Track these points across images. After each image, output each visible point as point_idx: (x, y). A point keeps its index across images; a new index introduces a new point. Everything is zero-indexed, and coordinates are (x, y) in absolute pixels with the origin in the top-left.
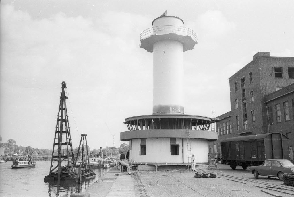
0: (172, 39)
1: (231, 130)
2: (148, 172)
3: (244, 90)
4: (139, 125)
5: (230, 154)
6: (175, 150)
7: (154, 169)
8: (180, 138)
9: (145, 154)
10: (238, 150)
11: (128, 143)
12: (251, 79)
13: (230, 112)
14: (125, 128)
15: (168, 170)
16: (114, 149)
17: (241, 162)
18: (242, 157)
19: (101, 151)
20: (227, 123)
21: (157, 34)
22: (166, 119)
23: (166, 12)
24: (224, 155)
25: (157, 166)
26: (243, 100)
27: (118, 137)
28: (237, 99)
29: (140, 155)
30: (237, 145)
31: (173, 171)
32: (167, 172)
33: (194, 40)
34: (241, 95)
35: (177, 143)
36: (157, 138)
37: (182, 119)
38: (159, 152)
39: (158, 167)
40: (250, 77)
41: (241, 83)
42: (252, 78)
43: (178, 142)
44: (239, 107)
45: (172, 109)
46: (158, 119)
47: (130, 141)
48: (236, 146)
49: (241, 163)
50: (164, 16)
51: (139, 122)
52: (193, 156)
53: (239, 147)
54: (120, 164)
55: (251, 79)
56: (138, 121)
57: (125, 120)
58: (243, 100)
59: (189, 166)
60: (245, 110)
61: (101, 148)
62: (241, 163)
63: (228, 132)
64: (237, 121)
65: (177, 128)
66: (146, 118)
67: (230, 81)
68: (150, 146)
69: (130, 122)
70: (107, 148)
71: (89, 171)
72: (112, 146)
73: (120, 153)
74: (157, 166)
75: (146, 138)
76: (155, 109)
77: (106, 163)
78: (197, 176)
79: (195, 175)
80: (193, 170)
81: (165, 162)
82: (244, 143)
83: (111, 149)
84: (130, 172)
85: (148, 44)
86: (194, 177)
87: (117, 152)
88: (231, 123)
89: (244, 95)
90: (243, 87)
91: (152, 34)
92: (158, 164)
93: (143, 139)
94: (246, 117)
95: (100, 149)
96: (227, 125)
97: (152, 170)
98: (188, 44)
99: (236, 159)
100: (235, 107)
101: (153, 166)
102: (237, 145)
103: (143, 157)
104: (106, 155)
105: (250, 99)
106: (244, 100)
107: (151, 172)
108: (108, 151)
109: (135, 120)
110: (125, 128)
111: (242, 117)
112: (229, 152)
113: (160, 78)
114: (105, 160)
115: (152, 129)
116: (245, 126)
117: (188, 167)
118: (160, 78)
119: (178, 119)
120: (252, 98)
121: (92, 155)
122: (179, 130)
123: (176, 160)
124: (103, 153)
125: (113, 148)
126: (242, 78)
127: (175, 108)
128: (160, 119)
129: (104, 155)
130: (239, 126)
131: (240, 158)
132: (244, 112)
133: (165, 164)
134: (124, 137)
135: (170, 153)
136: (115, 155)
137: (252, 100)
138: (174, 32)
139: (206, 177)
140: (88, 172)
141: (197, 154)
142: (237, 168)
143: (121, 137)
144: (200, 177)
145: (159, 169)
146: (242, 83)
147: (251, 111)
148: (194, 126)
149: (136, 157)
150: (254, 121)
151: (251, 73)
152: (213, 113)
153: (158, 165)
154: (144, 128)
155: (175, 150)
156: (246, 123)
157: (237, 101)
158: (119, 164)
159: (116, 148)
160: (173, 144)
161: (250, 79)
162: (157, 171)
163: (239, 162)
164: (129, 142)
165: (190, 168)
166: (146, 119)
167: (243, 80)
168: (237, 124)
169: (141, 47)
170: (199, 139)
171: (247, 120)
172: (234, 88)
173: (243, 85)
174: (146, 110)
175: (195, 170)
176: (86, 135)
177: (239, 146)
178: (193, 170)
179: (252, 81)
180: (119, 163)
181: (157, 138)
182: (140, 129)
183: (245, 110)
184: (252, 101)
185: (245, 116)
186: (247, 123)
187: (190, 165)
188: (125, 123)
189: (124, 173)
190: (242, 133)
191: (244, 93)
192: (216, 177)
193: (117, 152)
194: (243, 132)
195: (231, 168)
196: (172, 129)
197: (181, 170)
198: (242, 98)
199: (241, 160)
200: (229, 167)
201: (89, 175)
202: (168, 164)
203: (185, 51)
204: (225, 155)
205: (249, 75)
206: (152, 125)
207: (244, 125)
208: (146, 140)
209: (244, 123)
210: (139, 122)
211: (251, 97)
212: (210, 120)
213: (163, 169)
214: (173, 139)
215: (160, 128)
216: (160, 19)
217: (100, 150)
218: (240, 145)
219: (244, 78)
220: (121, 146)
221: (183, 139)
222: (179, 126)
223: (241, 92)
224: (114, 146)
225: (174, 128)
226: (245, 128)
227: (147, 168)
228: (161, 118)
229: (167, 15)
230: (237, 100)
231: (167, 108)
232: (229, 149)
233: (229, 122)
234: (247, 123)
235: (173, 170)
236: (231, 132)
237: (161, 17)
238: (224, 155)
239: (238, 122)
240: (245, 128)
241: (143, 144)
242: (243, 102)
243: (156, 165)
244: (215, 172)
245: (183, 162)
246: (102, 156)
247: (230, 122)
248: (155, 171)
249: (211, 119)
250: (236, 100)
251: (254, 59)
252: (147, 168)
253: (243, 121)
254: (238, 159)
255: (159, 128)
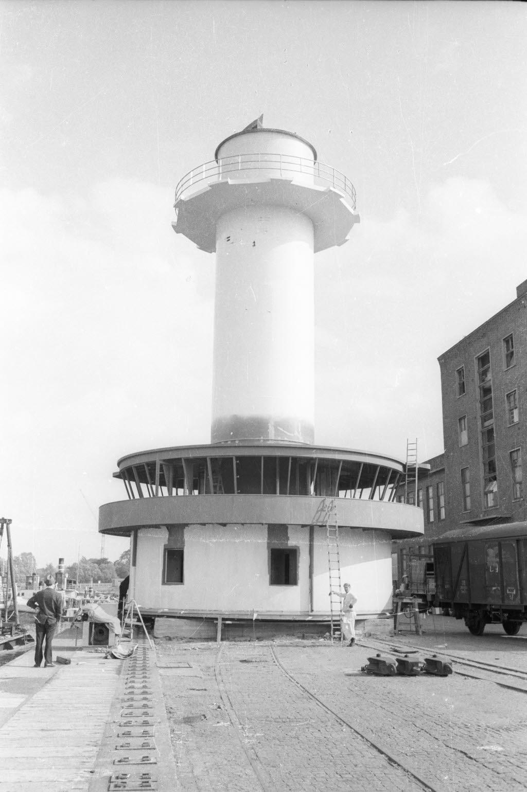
0: (276, 200)
1: (443, 511)
2: (193, 645)
3: (486, 391)
4: (162, 483)
5: (464, 582)
6: (283, 568)
7: (211, 634)
8: (303, 526)
9: (181, 580)
10: (494, 568)
11: (123, 544)
12: (510, 355)
13: (442, 456)
14: (118, 491)
15: (259, 634)
16: (103, 565)
17: (505, 611)
18: (512, 592)
19: (63, 570)
20: (431, 490)
21: (230, 182)
22: (256, 459)
23: (261, 118)
24: (443, 586)
25: (220, 622)
26: (484, 419)
27: (93, 522)
28: (464, 417)
29: (164, 583)
30: (492, 552)
31: (277, 641)
32: (256, 643)
33: (352, 210)
34: (478, 405)
35: (292, 543)
36: (224, 525)
37: (310, 461)
38: (227, 572)
39: (225, 625)
40: (508, 350)
41: (476, 367)
42: (512, 353)
43: (296, 540)
44: (469, 442)
45: (276, 430)
46: (227, 461)
47: (132, 537)
48: (487, 555)
49: (506, 615)
50: (253, 128)
51: (161, 470)
52: (346, 586)
53: (501, 558)
54: (85, 617)
55: (510, 355)
56: (161, 465)
57: (119, 464)
58: (484, 419)
59: (332, 623)
60: (490, 450)
61: (61, 560)
62: (506, 615)
63: (435, 518)
64: (464, 482)
65: (293, 492)
66: (191, 455)
67: (441, 365)
68: (195, 550)
69: (135, 470)
70: (84, 561)
71: (14, 631)
72: (99, 558)
73: (120, 576)
74: (220, 622)
75: (187, 525)
76: (218, 429)
77: (74, 602)
78: (374, 668)
79: (368, 663)
80: (349, 637)
81: (250, 609)
82: (518, 545)
83: (96, 565)
84: (121, 649)
85: (200, 220)
86: (363, 669)
87: (111, 573)
88: (442, 491)
89: (486, 405)
90: (483, 381)
91: (215, 180)
92: (226, 617)
93: (176, 529)
94: (494, 471)
95: (60, 563)
96: (431, 495)
97: (204, 635)
98: (326, 221)
99: (490, 601)
100: (457, 441)
101: (210, 621)
102: (492, 552)
103: (174, 589)
104: (75, 582)
105: (507, 416)
106: (485, 421)
107: (198, 645)
108: (85, 570)
109: (148, 464)
110: (118, 491)
111: (481, 473)
112: (464, 575)
113: (238, 325)
114: (73, 595)
115: (206, 493)
116: (490, 496)
117: (329, 626)
118: (238, 325)
119: (295, 459)
120: (512, 413)
121: (33, 580)
122: (301, 500)
123: (287, 602)
124: (67, 575)
125: (102, 562)
126: (480, 353)
127: (282, 425)
128: (234, 460)
129: (69, 582)
130: (468, 500)
131: (504, 596)
132: (487, 455)
133: (249, 617)
134: (114, 523)
135: (267, 578)
136: (106, 580)
137: (513, 417)
138: (285, 176)
139: (413, 674)
140: (11, 634)
141: (358, 582)
142: (489, 628)
143: (101, 523)
144: (387, 672)
145: (231, 633)
146: (482, 370)
147: (511, 453)
148: (345, 491)
149: (150, 590)
150: (520, 483)
151: (512, 338)
152: (410, 447)
153: (224, 619)
154: (181, 492)
155: (283, 568)
156: (494, 487)
157: (465, 423)
158: (80, 618)
159: (108, 563)
160: (278, 544)
161: (507, 356)
162: (222, 640)
163: (497, 610)
164: (129, 538)
165: (338, 627)
166: (188, 460)
167: (484, 360)
168: (465, 492)
169: (178, 228)
170: (365, 529)
171: (495, 478)
172: (456, 386)
173: (484, 373)
174: (189, 427)
175: (353, 640)
176: (10, 520)
177: (499, 555)
178: (349, 637)
179: (514, 362)
180: (81, 613)
181: (224, 525)
182: (166, 494)
183: (490, 450)
184: (513, 422)
185: (491, 466)
186: (495, 490)
187: (338, 618)
188: (117, 476)
189: (96, 651)
190: (482, 517)
191: (486, 398)
192: (450, 672)
193: (111, 573)
194: (484, 516)
195: (467, 629)
196: (275, 493)
197: (303, 637)
198: (479, 413)
199: (507, 602)
200: (461, 625)
201: (11, 644)
202: (260, 618)
203: (317, 252)
204: (447, 586)
205: (503, 345)
206: (208, 480)
207: (486, 494)
208: (186, 530)
209: (485, 488)
210: (164, 468)
211: (511, 411)
212: (400, 468)
213: (241, 634)
214: (278, 530)
215: (236, 492)
216: (244, 138)
217: (60, 567)
218: (503, 552)
219: (488, 353)
220: (122, 557)
221: (311, 529)
222: (298, 482)
223: (478, 397)
224: (106, 557)
225: (283, 492)
226: (491, 503)
227: (185, 628)
228: (238, 458)
229: (265, 125)
230: (463, 421)
231: (259, 425)
232: (462, 560)
233: (438, 488)
234: (495, 490)
235: (273, 636)
236: (443, 516)
237: (246, 131)
238: (443, 586)
239: (468, 486)
240: (491, 503)
241: (176, 547)
242: (483, 426)
243: (217, 619)
244: (445, 653)
245: (312, 611)
246: (65, 586)
247: (441, 486)
248: (214, 639)
249: (404, 466)
250: (460, 420)
251: (518, 297)
252: (186, 628)
253: (482, 482)
254: (494, 601)
255: (229, 490)
